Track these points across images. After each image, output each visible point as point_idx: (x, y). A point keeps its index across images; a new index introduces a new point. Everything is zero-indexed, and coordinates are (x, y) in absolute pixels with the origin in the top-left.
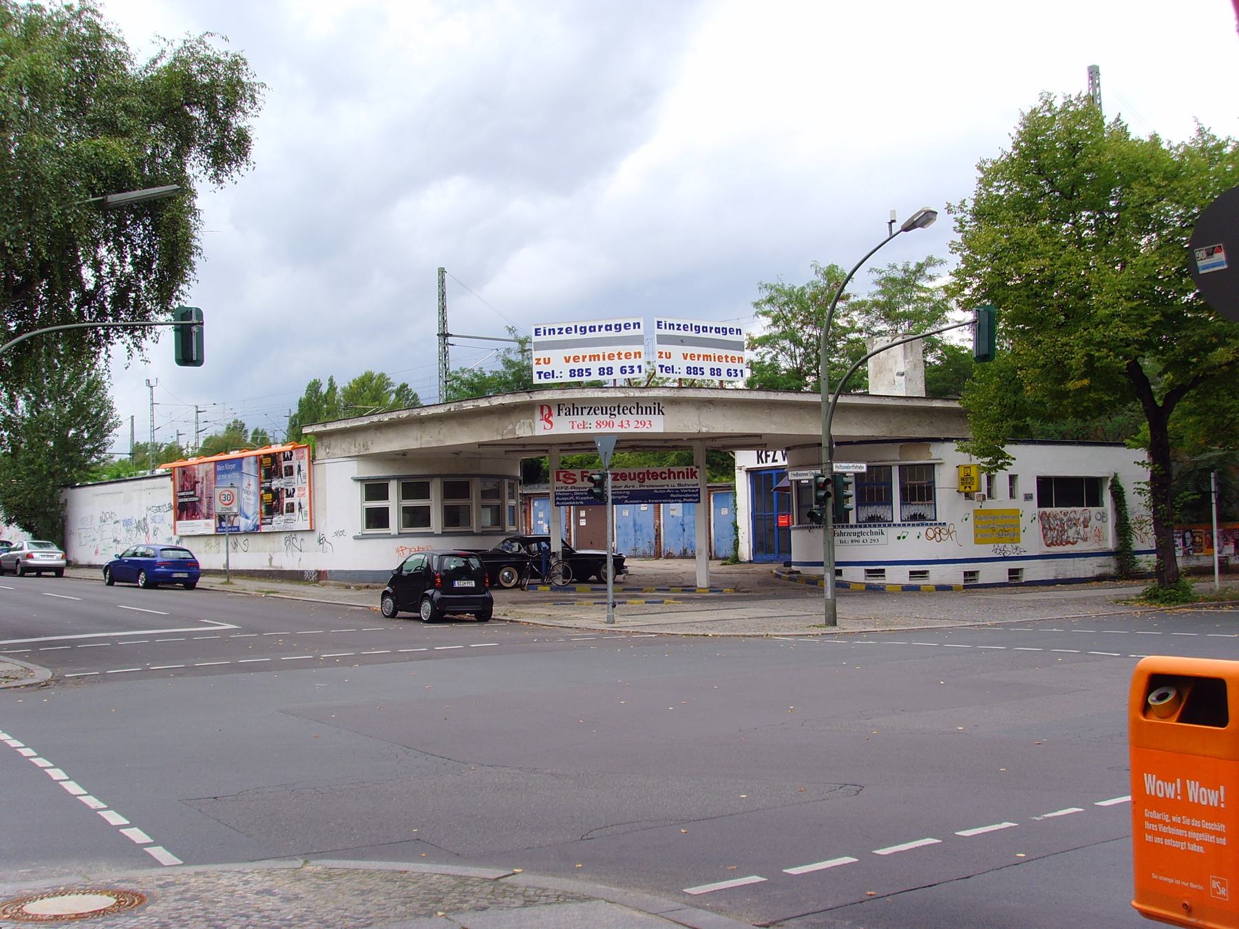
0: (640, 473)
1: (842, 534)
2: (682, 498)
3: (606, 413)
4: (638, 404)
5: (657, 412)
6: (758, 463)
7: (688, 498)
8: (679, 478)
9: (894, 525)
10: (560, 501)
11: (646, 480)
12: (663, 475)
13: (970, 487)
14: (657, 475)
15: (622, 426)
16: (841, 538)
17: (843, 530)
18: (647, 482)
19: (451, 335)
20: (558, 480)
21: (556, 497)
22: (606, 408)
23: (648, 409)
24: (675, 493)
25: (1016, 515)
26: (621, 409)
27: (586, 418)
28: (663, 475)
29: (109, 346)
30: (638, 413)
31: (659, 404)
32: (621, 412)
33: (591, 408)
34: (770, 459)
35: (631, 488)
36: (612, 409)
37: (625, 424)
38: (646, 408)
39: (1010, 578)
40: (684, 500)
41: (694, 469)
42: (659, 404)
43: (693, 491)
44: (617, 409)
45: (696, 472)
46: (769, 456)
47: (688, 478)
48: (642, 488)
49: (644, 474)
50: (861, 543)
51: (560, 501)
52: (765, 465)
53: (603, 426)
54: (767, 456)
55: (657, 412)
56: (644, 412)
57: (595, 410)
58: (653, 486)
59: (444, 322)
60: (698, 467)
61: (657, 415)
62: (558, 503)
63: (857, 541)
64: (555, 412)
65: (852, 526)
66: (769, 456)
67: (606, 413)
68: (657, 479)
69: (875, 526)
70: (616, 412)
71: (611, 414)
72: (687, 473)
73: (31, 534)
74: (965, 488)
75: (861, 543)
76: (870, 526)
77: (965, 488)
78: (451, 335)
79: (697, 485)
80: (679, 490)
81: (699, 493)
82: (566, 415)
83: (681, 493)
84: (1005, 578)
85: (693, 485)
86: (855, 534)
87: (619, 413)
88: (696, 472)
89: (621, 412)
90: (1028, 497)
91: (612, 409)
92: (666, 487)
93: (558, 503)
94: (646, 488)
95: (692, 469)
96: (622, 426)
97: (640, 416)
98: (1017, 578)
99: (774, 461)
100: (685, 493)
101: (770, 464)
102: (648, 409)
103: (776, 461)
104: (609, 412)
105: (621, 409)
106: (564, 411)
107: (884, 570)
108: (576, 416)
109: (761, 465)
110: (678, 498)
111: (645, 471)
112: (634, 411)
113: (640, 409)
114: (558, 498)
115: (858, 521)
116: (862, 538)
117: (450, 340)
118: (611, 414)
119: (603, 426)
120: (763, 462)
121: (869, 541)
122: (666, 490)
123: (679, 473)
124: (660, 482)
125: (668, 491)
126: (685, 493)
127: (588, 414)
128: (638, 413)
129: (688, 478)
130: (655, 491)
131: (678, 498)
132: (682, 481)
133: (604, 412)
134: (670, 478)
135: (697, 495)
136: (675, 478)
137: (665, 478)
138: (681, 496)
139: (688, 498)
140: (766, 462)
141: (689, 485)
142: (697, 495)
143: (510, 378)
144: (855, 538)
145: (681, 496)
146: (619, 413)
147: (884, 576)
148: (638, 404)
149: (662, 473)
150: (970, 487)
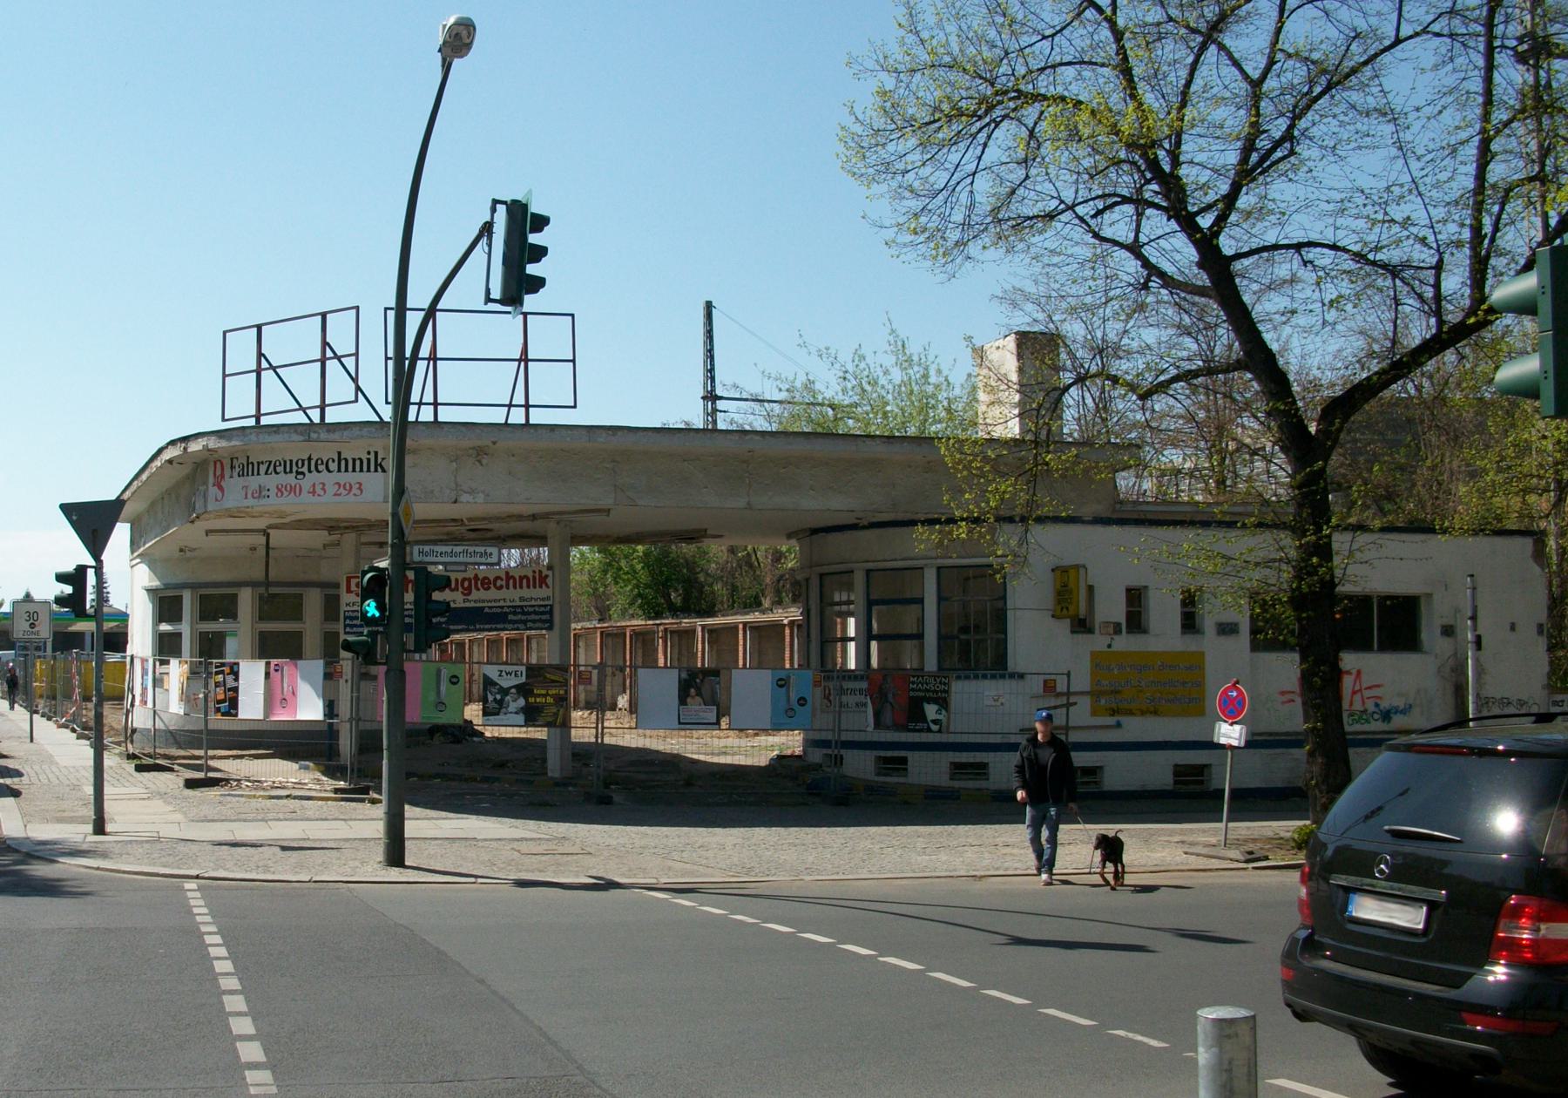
0: (464, 580)
2: (524, 622)
3: (291, 471)
4: (339, 453)
5: (372, 468)
7: (534, 621)
8: (521, 587)
10: (352, 626)
11: (474, 590)
12: (499, 583)
15: (314, 493)
18: (475, 595)
19: (721, 398)
20: (349, 591)
21: (345, 618)
22: (291, 461)
23: (358, 463)
24: (515, 613)
25: (1195, 664)
26: (313, 463)
27: (263, 479)
30: (339, 471)
31: (376, 453)
32: (313, 468)
33: (270, 462)
36: (300, 465)
37: (318, 489)
38: (354, 460)
39: (1176, 782)
40: (529, 625)
42: (376, 453)
43: (542, 609)
44: (306, 463)
45: (547, 576)
47: (535, 587)
48: (467, 605)
49: (469, 580)
51: (352, 626)
53: (286, 493)
55: (372, 468)
56: (350, 468)
58: (483, 601)
59: (710, 373)
61: (372, 475)
62: (348, 629)
63: (292, 489)
67: (291, 471)
68: (488, 588)
70: (305, 469)
71: (298, 473)
72: (534, 578)
73: (1343, 588)
78: (721, 398)
79: (548, 598)
80: (521, 607)
83: (523, 613)
84: (1164, 780)
85: (543, 599)
87: (310, 471)
88: (547, 576)
89: (313, 468)
90: (1227, 629)
91: (300, 465)
92: (502, 603)
93: (348, 629)
94: (472, 605)
96: (314, 493)
98: (1202, 782)
100: (529, 613)
102: (358, 463)
104: (295, 469)
105: (313, 463)
106: (238, 469)
107: (904, 760)
108: (250, 478)
110: (521, 621)
111: (472, 576)
112: (333, 466)
113: (343, 463)
114: (348, 622)
117: (720, 405)
118: (298, 473)
119: (286, 493)
121: (331, 489)
122: (502, 607)
123: (521, 578)
124: (493, 593)
125: (506, 610)
126: (529, 613)
127: (266, 473)
128: (339, 471)
129: (535, 587)
130: (487, 610)
131: (521, 621)
132: (526, 593)
133: (288, 470)
134: (508, 588)
135: (546, 617)
136: (515, 587)
137: (501, 587)
138: (524, 618)
139: (534, 621)
141: (536, 600)
142: (546, 617)
143: (1463, 489)
145: (524, 618)
146: (310, 471)
147: (906, 769)
148: (339, 453)
149: (498, 578)
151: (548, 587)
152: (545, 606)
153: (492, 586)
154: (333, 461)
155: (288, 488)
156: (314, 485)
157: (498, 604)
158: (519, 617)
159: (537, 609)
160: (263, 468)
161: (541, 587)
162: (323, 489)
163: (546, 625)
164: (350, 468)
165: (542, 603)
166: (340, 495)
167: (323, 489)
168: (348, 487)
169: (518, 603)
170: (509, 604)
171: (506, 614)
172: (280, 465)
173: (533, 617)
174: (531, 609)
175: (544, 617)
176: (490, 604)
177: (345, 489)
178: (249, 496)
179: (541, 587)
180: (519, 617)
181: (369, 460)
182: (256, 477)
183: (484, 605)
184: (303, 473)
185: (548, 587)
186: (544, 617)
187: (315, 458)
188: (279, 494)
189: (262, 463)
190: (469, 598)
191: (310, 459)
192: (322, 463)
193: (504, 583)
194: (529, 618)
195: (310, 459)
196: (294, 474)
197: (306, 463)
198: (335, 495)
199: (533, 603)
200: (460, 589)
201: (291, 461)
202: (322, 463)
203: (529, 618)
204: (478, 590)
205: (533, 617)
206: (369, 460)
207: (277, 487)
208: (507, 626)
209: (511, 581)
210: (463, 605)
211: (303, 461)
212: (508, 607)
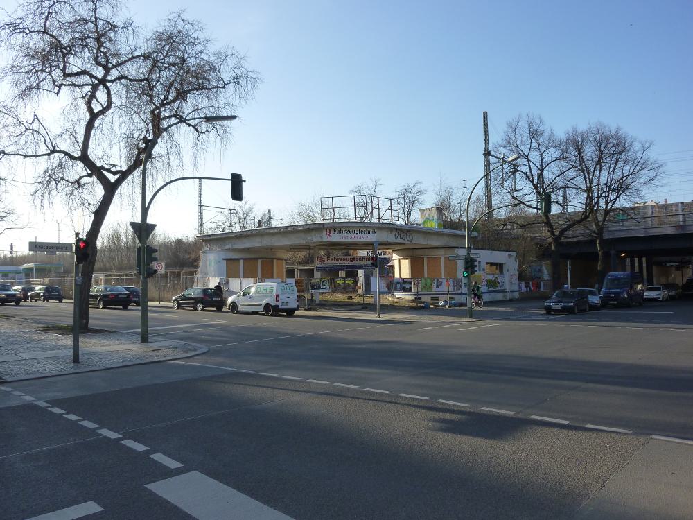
64: (332, 231)
117: (203, 207)
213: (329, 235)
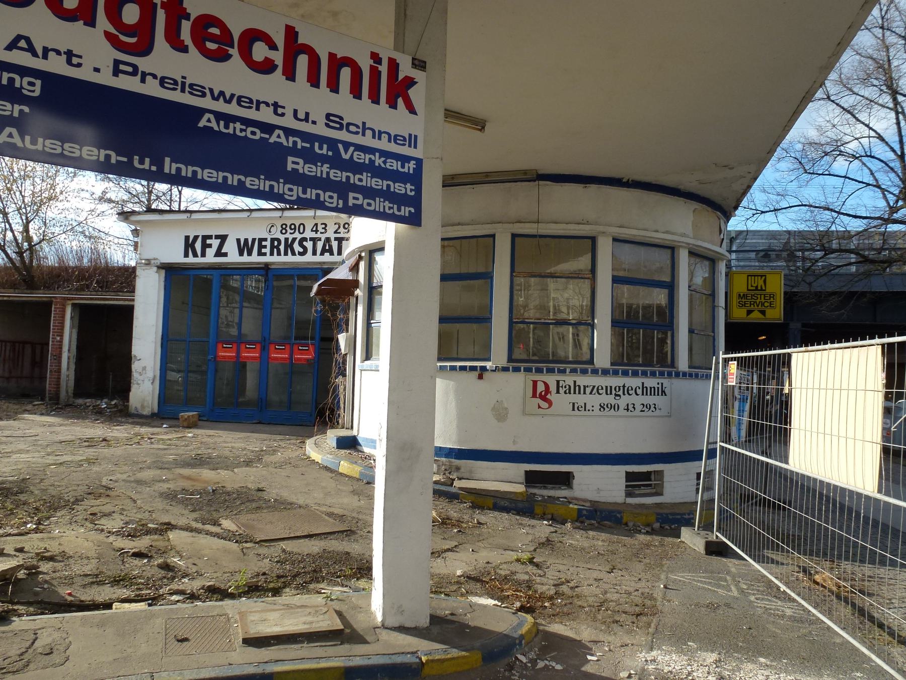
1: (576, 389)
2: (343, 189)
3: (611, 394)
5: (660, 394)
6: (186, 255)
8: (334, 86)
9: (677, 375)
12: (260, 51)
13: (763, 313)
14: (226, 37)
15: (628, 410)
16: (572, 398)
17: (582, 380)
22: (611, 387)
24: (310, 157)
26: (626, 389)
28: (260, 51)
29: (47, 483)
34: (210, 252)
35: (56, 65)
36: (617, 390)
37: (631, 407)
38: (651, 388)
40: (353, 199)
41: (406, 70)
43: (394, 165)
44: (622, 388)
46: (210, 246)
50: (622, 412)
52: (199, 260)
54: (205, 246)
55: (660, 394)
56: (649, 393)
57: (598, 389)
58: (197, 90)
60: (419, 64)
65: (595, 372)
66: (210, 246)
67: (611, 394)
68: (221, 56)
69: (653, 374)
70: (621, 393)
71: (616, 395)
72: (375, 74)
74: (749, 312)
75: (622, 412)
76: (644, 374)
77: (749, 312)
79: (412, 141)
80: (332, 143)
81: (416, 179)
82: (565, 393)
83: (337, 162)
86: (609, 390)
87: (624, 394)
88: (410, 82)
91: (617, 390)
92: (266, 115)
94: (152, 89)
95: (393, 66)
96: (628, 410)
97: (645, 396)
99: (219, 253)
101: (210, 257)
103: (225, 255)
109: (191, 259)
110: (325, 184)
112: (639, 391)
115: (510, 360)
116: (624, 400)
118: (616, 395)
120: (195, 255)
121: (639, 407)
122: (268, 128)
127: (591, 393)
128: (643, 394)
129: (375, 98)
131: (325, 184)
133: (609, 393)
136: (314, 80)
137: (266, 67)
138: (337, 175)
140: (203, 254)
144: (610, 399)
145: (337, 175)
146: (624, 394)
149: (252, 36)
150: (763, 313)
151: (412, 110)
152: (405, 159)
153: (234, 52)
154: (639, 388)
155: (609, 406)
156: (628, 405)
157: (251, 114)
158: (324, 169)
159: (379, 161)
160: (588, 390)
161: (393, 105)
162: (634, 408)
163: (406, 211)
164: (649, 393)
165: (393, 148)
166: (644, 411)
167: (634, 408)
168: (648, 407)
169: (320, 129)
170: (288, 122)
171: (283, 152)
172: (602, 389)
173: (366, 180)
174: (361, 158)
175: (399, 188)
176: (221, 106)
177: (647, 407)
178: (576, 409)
179: (393, 105)
180: (324, 169)
181: (658, 388)
182: (582, 396)
183: (206, 103)
184: (619, 396)
185: (412, 110)
186: (399, 188)
187: (627, 386)
188: (602, 409)
189: (588, 386)
190: (143, 63)
191: (624, 386)
192: (632, 389)
193: (278, 57)
194: (354, 179)
195: (624, 386)
196: (613, 396)
197: (622, 388)
198: (641, 411)
199: (368, 141)
200: (103, 22)
201: (611, 387)
202: (632, 389)
203: (354, 179)
204: (184, 49)
205: (366, 180)
206: (658, 388)
207: (600, 405)
208: (280, 187)
209: (302, 61)
210: (106, 79)
211: (619, 387)
212: (288, 132)
213: (544, 398)
